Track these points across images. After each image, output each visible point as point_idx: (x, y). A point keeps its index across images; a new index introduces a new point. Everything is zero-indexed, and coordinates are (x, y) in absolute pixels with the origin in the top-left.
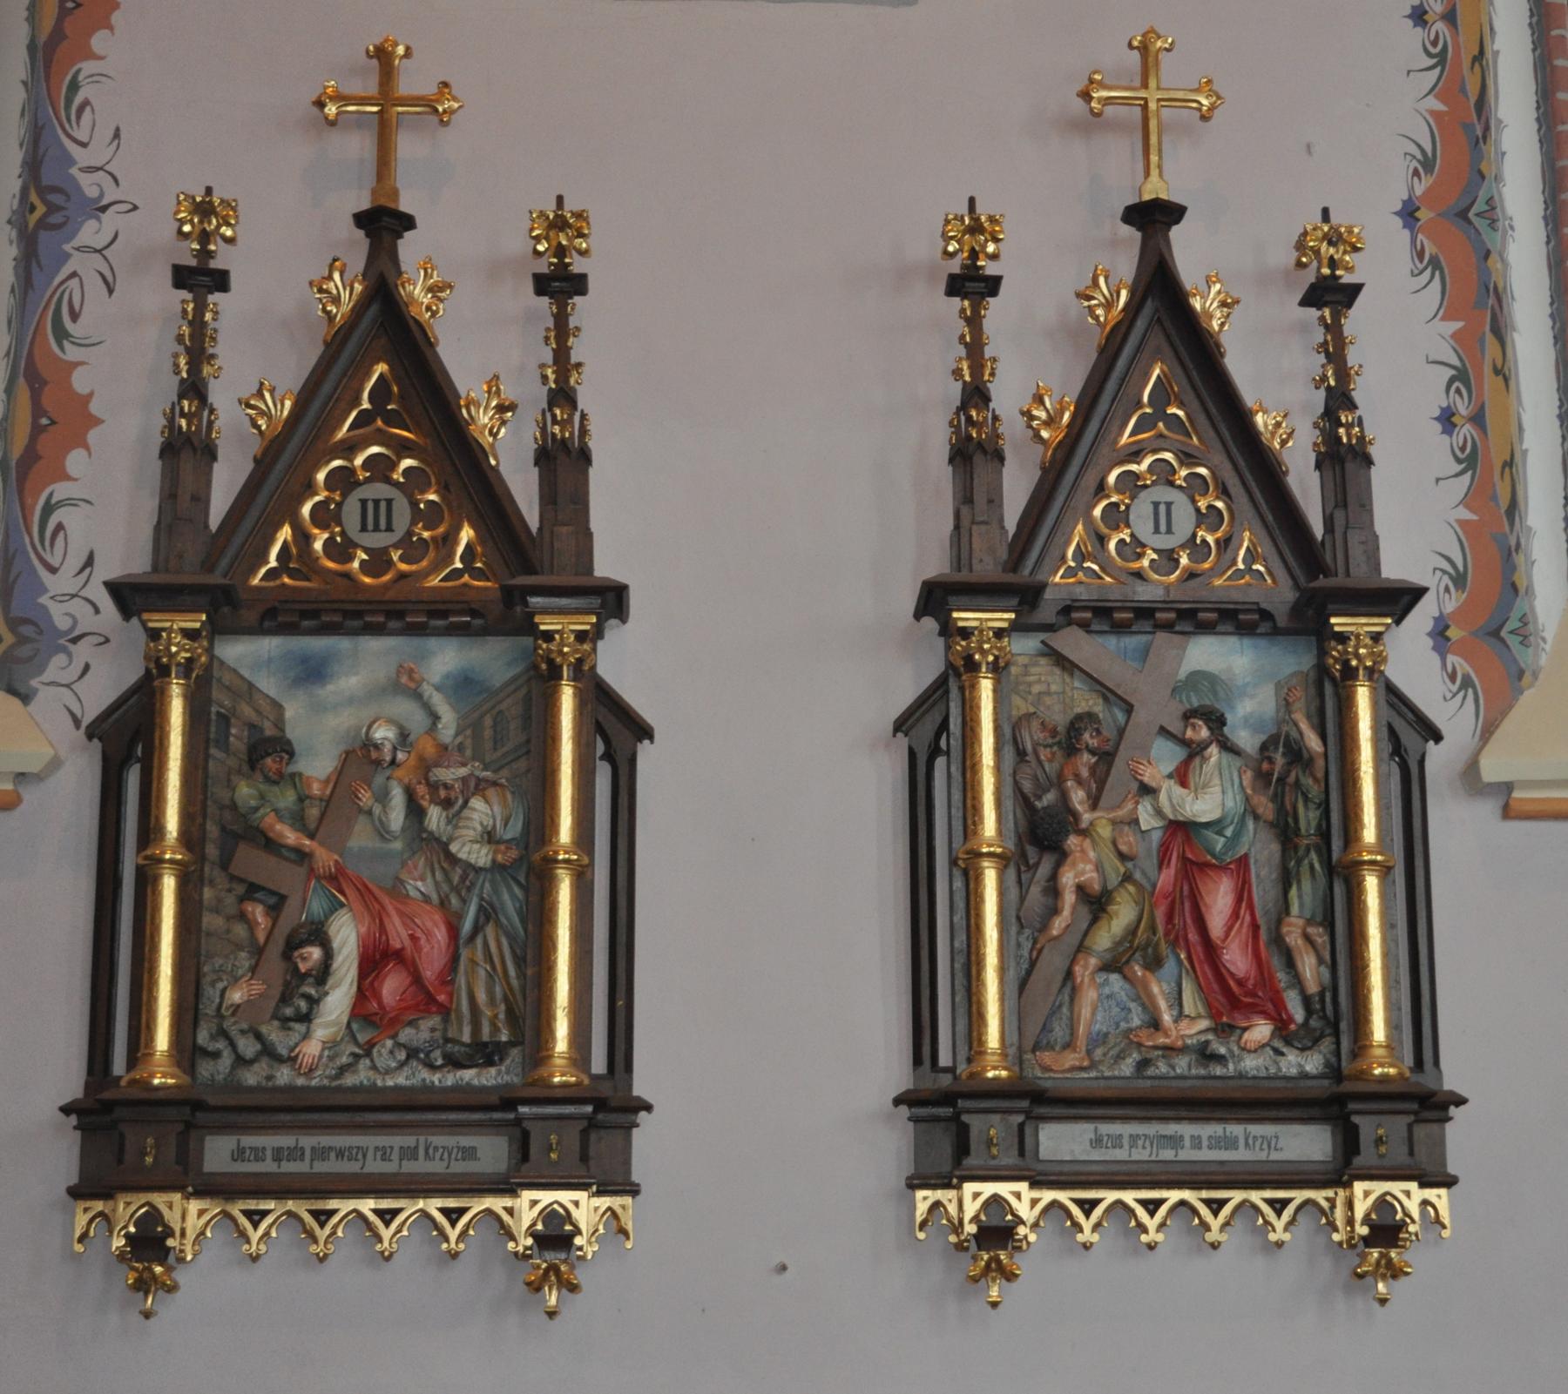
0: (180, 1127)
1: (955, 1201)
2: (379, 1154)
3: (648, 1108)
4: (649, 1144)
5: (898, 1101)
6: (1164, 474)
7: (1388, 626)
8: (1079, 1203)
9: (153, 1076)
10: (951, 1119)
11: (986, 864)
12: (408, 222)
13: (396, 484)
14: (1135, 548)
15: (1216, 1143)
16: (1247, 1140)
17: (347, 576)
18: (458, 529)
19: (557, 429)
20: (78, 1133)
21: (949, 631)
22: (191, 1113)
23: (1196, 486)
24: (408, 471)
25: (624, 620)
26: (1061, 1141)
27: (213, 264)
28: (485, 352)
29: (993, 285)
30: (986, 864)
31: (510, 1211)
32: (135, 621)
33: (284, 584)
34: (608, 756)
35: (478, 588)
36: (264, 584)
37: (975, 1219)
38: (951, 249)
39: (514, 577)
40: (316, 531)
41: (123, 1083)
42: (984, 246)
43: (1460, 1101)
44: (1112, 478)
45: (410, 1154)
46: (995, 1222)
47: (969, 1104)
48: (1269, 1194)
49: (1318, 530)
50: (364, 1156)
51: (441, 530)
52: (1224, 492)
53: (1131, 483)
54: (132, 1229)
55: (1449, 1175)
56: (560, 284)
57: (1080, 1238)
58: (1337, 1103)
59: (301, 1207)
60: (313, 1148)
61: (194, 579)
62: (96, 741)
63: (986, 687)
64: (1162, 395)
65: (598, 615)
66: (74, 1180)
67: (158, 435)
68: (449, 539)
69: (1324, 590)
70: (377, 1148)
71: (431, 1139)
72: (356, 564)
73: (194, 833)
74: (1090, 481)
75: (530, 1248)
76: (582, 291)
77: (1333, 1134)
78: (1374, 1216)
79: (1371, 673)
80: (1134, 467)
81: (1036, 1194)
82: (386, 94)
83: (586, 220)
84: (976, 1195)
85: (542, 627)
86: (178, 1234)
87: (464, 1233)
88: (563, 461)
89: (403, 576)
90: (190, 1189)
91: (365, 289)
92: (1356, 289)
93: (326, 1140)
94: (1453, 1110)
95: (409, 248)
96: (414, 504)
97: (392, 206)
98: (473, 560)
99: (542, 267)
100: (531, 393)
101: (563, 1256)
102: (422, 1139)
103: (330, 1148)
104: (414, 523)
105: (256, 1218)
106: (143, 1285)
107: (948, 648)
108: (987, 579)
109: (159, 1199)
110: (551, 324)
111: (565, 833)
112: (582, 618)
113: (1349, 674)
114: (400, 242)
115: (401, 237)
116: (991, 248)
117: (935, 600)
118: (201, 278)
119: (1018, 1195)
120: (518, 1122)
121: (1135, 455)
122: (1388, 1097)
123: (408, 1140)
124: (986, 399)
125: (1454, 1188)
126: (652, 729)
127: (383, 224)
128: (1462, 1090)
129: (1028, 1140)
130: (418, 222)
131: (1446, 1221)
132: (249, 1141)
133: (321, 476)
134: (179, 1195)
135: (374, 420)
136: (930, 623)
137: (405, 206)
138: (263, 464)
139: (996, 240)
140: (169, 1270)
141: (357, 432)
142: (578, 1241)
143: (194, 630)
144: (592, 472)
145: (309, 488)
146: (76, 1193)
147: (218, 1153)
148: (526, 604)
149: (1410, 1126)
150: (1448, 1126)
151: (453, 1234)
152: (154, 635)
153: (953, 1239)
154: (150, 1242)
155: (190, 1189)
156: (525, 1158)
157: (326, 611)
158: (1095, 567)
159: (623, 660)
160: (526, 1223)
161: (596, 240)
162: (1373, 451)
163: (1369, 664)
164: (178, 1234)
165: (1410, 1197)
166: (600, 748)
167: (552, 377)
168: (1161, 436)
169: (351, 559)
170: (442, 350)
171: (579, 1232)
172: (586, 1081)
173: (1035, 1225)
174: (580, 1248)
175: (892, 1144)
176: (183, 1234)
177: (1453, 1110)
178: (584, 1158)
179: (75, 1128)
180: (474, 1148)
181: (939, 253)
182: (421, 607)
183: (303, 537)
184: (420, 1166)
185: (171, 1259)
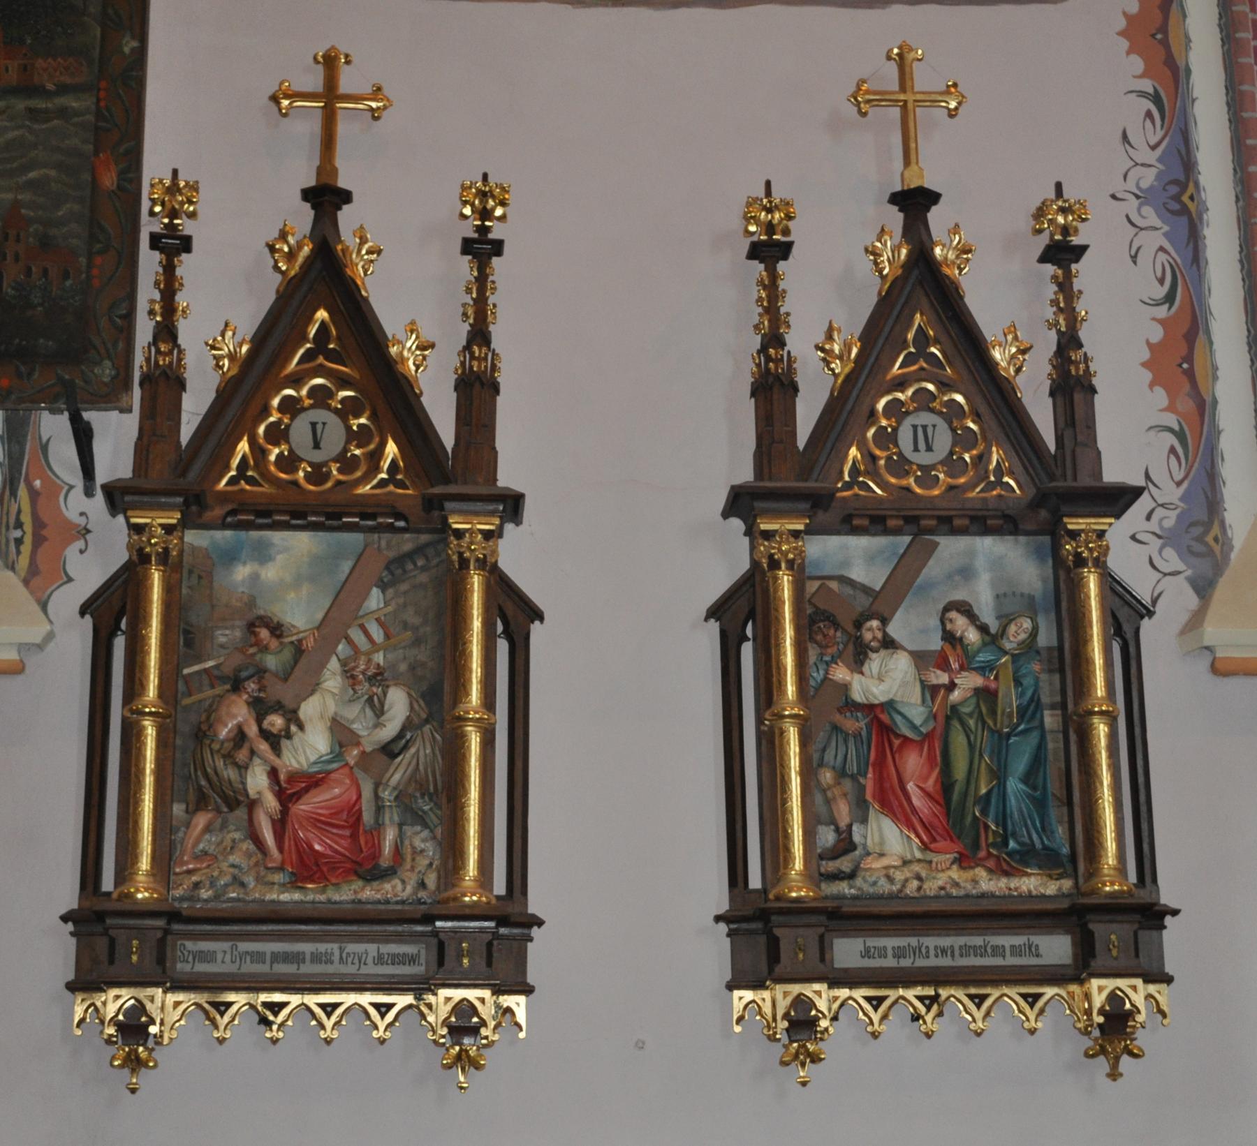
1: (769, 1003)
3: (540, 923)
4: (541, 953)
6: (924, 401)
7: (1110, 524)
10: (765, 934)
11: (146, 723)
12: (346, 197)
14: (288, 462)
15: (882, 953)
17: (295, 483)
18: (383, 445)
19: (475, 364)
20: (73, 941)
23: (350, 409)
26: (848, 951)
27: (491, 236)
29: (497, 248)
32: (121, 519)
33: (243, 490)
34: (508, 634)
36: (229, 488)
39: (432, 486)
41: (115, 896)
42: (493, 209)
44: (881, 405)
46: (802, 1017)
47: (781, 919)
48: (919, 991)
49: (1052, 447)
50: (341, 958)
51: (372, 446)
52: (977, 418)
53: (895, 409)
54: (121, 1017)
55: (528, 985)
56: (482, 249)
57: (322, 1034)
58: (1078, 916)
59: (202, 998)
62: (88, 617)
63: (156, 577)
64: (923, 339)
65: (501, 518)
66: (71, 976)
68: (378, 453)
69: (1062, 495)
72: (301, 474)
74: (865, 409)
75: (443, 1037)
76: (499, 253)
77: (1074, 944)
78: (453, 1019)
79: (482, 563)
80: (900, 395)
82: (330, 94)
83: (197, 190)
84: (177, 1004)
85: (1070, 527)
86: (158, 1021)
87: (337, 1023)
88: (477, 390)
91: (312, 250)
92: (1083, 249)
94: (1168, 920)
95: (937, 218)
97: (331, 182)
105: (383, 1010)
107: (753, 548)
108: (785, 482)
111: (1100, 690)
112: (171, 514)
113: (1080, 561)
116: (499, 212)
117: (740, 503)
119: (1134, 988)
120: (435, 933)
121: (901, 384)
124: (781, 343)
125: (532, 996)
127: (326, 198)
128: (1173, 905)
130: (298, 195)
131: (1165, 1008)
132: (874, 942)
133: (276, 402)
134: (160, 990)
137: (342, 183)
138: (227, 394)
139: (503, 203)
142: (484, 1032)
146: (72, 987)
149: (822, 937)
150: (1165, 932)
151: (329, 1024)
152: (138, 529)
156: (441, 963)
157: (892, 517)
158: (1012, 483)
159: (517, 554)
161: (205, 203)
162: (1095, 381)
163: (791, 556)
164: (158, 1021)
165: (1137, 993)
168: (922, 369)
169: (296, 470)
173: (835, 1018)
174: (486, 1038)
179: (72, 934)
183: (259, 452)
185: (150, 1044)
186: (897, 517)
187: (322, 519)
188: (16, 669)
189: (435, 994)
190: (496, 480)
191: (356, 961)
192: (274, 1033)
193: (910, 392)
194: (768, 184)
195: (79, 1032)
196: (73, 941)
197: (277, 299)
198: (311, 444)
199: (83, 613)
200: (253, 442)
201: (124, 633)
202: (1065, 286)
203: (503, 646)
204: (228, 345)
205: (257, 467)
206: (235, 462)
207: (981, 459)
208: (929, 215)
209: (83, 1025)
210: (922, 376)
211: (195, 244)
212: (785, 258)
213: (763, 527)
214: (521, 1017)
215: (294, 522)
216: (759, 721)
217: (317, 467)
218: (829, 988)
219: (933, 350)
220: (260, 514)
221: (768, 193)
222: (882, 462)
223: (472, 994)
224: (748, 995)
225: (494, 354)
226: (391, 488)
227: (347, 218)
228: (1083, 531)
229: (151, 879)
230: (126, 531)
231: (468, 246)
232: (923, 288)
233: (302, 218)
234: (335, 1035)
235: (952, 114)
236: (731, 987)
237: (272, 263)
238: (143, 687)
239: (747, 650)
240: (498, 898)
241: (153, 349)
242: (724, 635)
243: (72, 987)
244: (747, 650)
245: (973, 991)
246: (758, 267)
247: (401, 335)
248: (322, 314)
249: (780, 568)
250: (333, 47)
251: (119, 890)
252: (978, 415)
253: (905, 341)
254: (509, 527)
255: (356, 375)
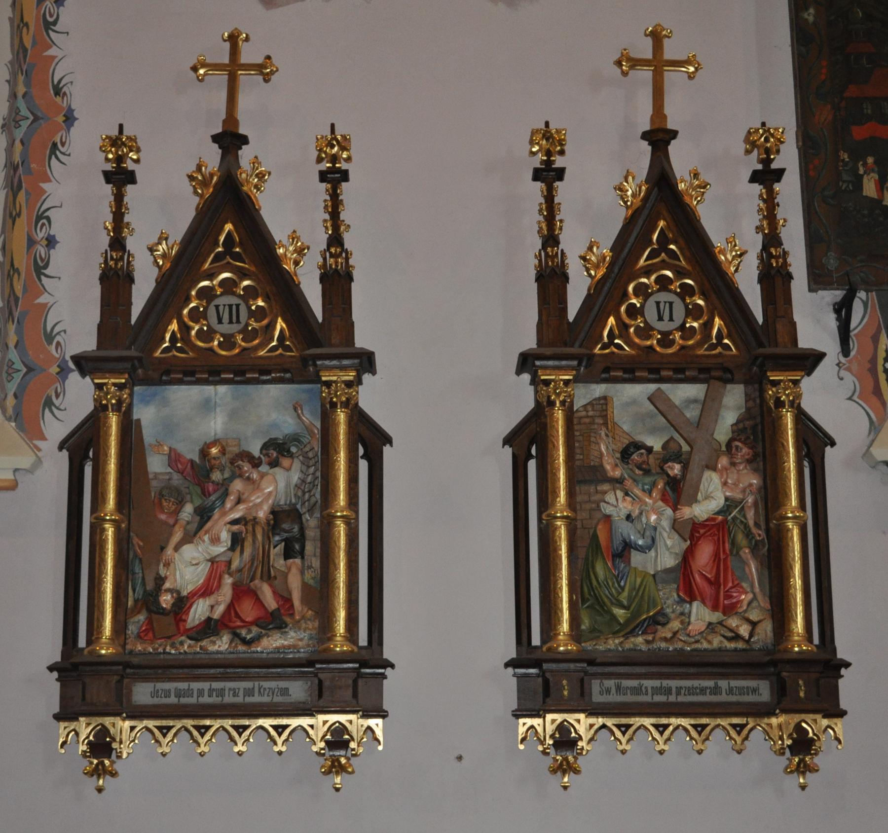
0: (354, 675)
2: (232, 692)
3: (392, 666)
4: (394, 687)
5: (507, 665)
8: (275, 727)
9: (559, 646)
12: (244, 140)
13: (240, 296)
15: (167, 694)
16: (260, 689)
17: (211, 349)
20: (58, 684)
21: (535, 381)
22: (128, 669)
24: (246, 288)
25: (374, 373)
28: (289, 213)
29: (560, 174)
30: (339, 522)
31: (312, 726)
32: (88, 379)
35: (182, 358)
37: (552, 736)
38: (534, 150)
40: (191, 324)
41: (86, 652)
43: (847, 665)
45: (249, 692)
48: (158, 723)
49: (760, 320)
52: (704, 295)
53: (641, 290)
54: (328, 737)
56: (334, 178)
60: (652, 688)
61: (130, 351)
64: (664, 240)
66: (56, 709)
67: (756, 268)
68: (271, 326)
70: (230, 689)
71: (262, 683)
72: (216, 343)
73: (119, 502)
79: (346, 405)
81: (592, 720)
84: (325, 722)
85: (771, 378)
86: (118, 740)
88: (338, 282)
89: (244, 349)
90: (124, 715)
93: (734, 683)
94: (843, 671)
95: (674, 148)
96: (249, 308)
98: (723, 339)
99: (109, 167)
100: (319, 239)
101: (343, 753)
102: (257, 683)
103: (706, 688)
104: (249, 318)
106: (99, 771)
107: (799, 396)
109: (107, 721)
110: (112, 198)
114: (240, 152)
115: (241, 148)
117: (526, 362)
118: (120, 177)
119: (578, 721)
122: (801, 663)
123: (248, 684)
124: (556, 243)
126: (391, 438)
127: (230, 140)
129: (586, 686)
131: (381, 739)
132: (161, 686)
133: (193, 293)
135: (225, 258)
136: (526, 377)
137: (670, 125)
138: (163, 282)
140: (113, 763)
141: (649, 262)
143: (121, 383)
144: (134, 287)
145: (188, 300)
146: (58, 717)
147: (143, 693)
148: (315, 365)
149: (355, 682)
150: (385, 681)
153: (540, 748)
154: (101, 746)
155: (124, 715)
156: (320, 695)
159: (372, 397)
160: (320, 735)
166: (361, 451)
167: (330, 228)
169: (212, 340)
170: (263, 212)
171: (353, 739)
172: (356, 650)
173: (591, 740)
174: (353, 750)
175: (506, 687)
176: (121, 742)
177: (843, 671)
178: (355, 695)
179: (57, 680)
180: (287, 689)
181: (528, 153)
182: (669, 366)
183: (185, 328)
184: (256, 699)
186: (669, 369)
187: (180, 376)
188: (13, 486)
189: (544, 718)
190: (354, 344)
191: (271, 694)
192: (203, 748)
193: (653, 277)
194: (333, 126)
195: (63, 751)
196: (58, 685)
197: (197, 214)
198: (657, 318)
199: (61, 448)
200: (618, 319)
201: (91, 460)
202: (119, 198)
203: (363, 465)
204: (162, 248)
205: (182, 339)
206: (168, 336)
207: (707, 326)
208: (669, 147)
209: (65, 747)
210: (665, 265)
211: (351, 176)
212: (779, 181)
213: (324, 379)
214: (379, 734)
215: (186, 379)
216: (540, 519)
217: (666, 334)
218: (586, 717)
219: (672, 247)
220: (186, 374)
221: (333, 131)
222: (632, 330)
223: (343, 718)
224: (529, 722)
225: (129, 255)
226: (280, 351)
227: (246, 155)
228: (334, 382)
229: (221, 634)
230: (93, 387)
231: (109, 177)
232: (228, 201)
233: (212, 157)
234: (284, 749)
235: (691, 76)
236: (517, 715)
237: (191, 189)
238: (104, 500)
239: (532, 465)
240: (816, 646)
241: (543, 254)
242: (514, 457)
243: (58, 717)
244: (532, 465)
245: (736, 721)
246: (757, 188)
247: (285, 242)
248: (229, 227)
249: (784, 407)
250: (236, 29)
251: (90, 648)
252: (268, 297)
253: (651, 240)
254: (366, 377)
255: (253, 269)
